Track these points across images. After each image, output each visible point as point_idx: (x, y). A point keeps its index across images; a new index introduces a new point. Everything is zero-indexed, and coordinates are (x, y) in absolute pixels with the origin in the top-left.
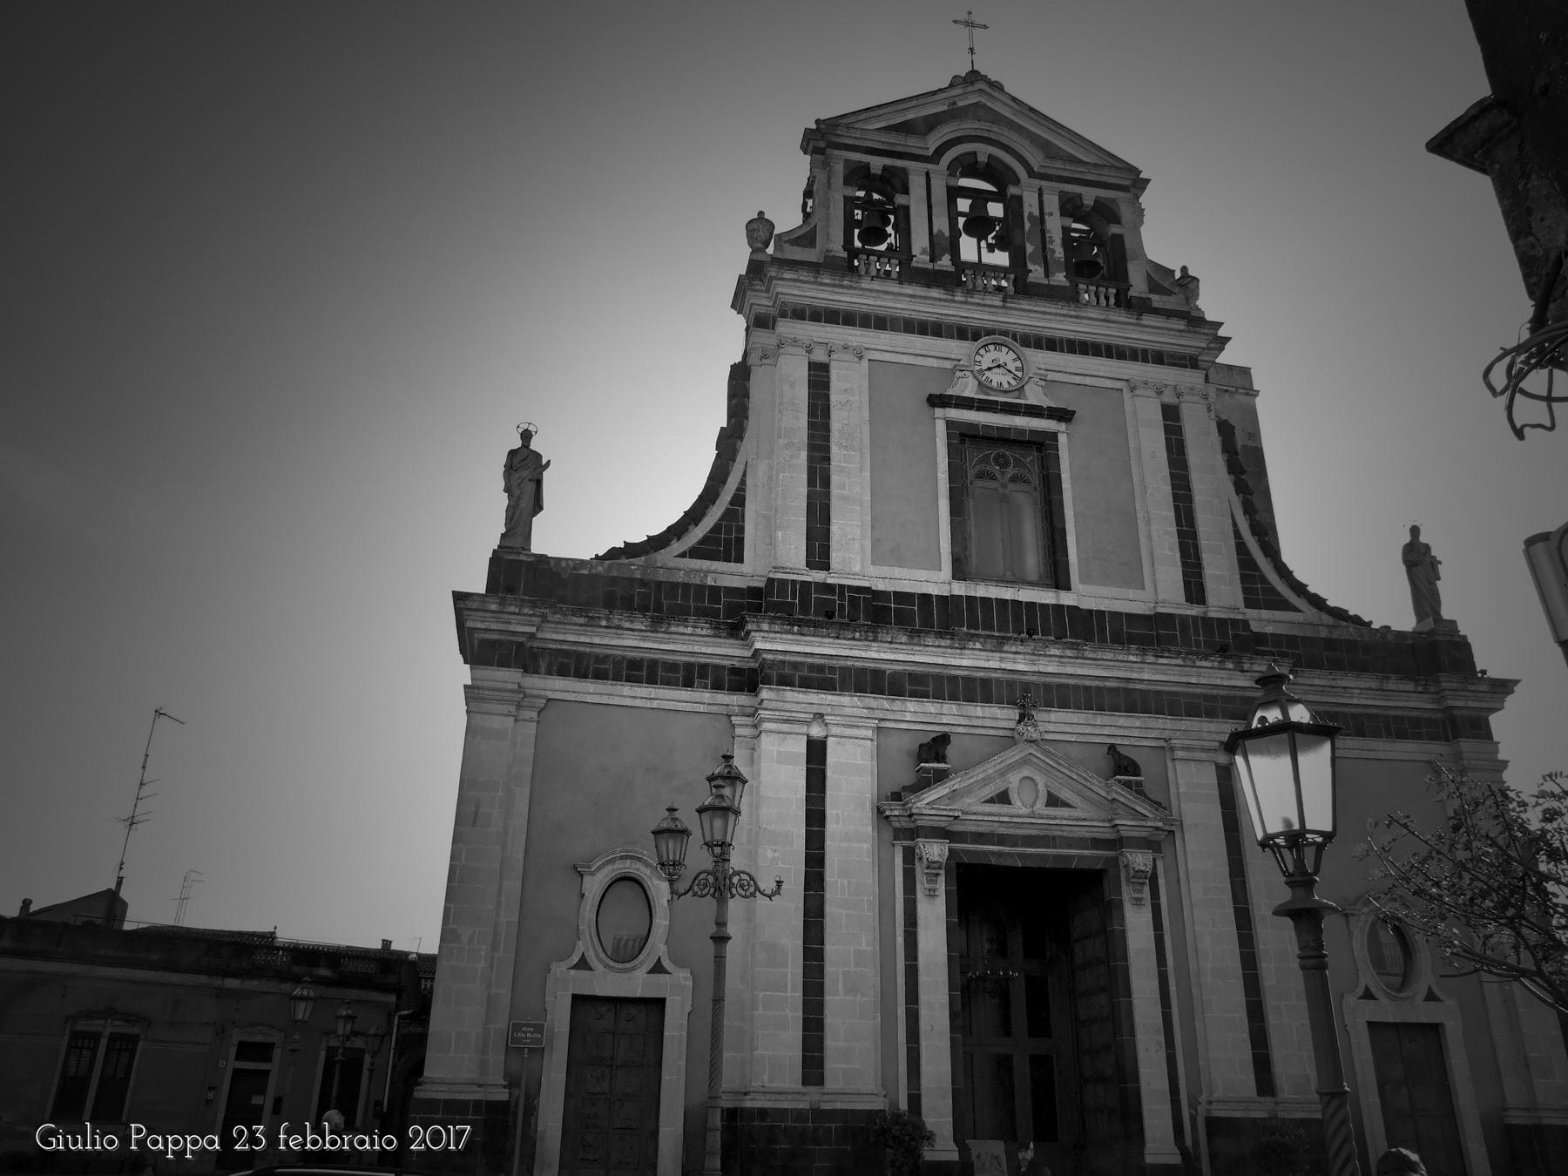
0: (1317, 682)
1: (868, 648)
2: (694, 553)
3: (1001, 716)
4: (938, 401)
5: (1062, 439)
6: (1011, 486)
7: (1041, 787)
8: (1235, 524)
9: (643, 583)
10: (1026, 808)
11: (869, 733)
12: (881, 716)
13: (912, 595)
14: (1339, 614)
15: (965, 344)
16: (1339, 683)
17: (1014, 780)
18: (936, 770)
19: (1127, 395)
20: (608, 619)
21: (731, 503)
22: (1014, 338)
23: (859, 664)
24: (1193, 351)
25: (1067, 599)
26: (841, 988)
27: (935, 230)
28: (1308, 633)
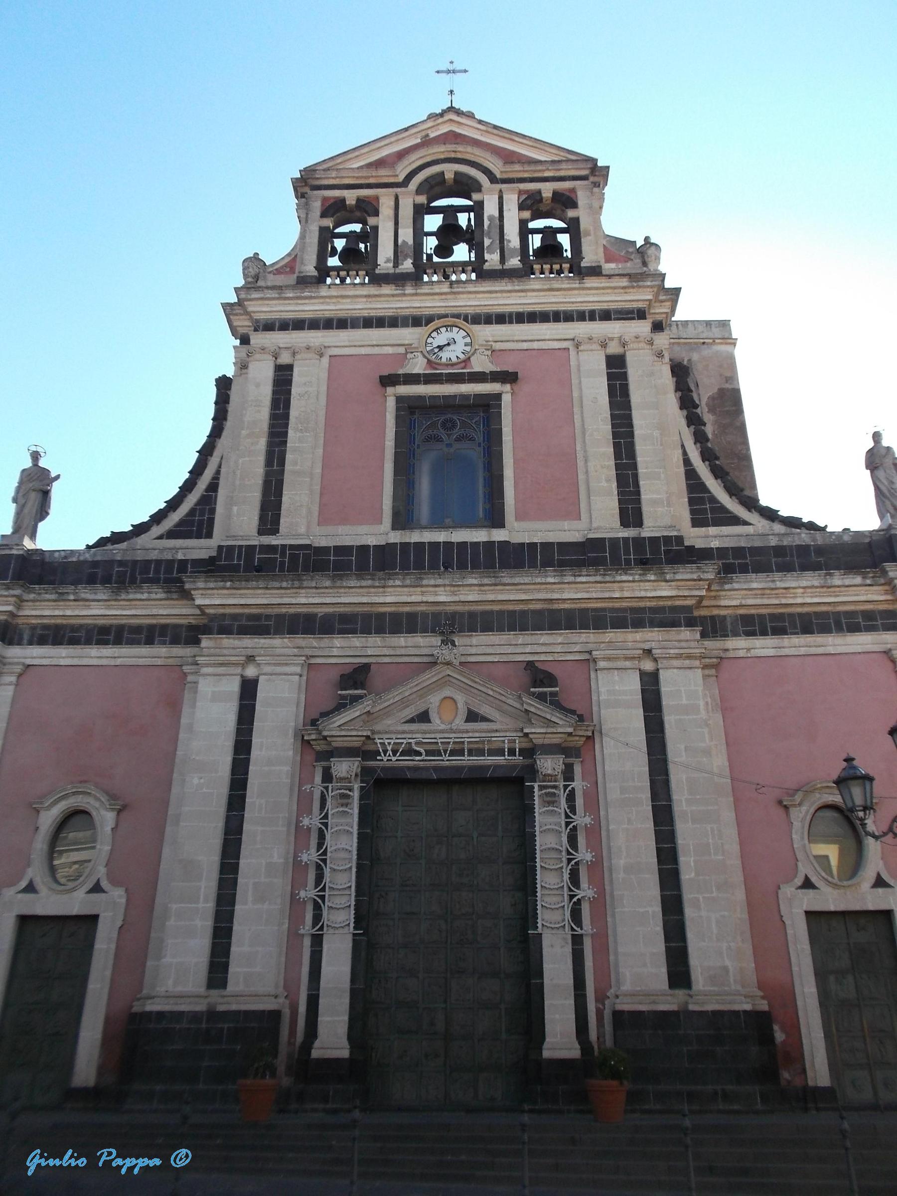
0: (755, 585)
1: (297, 594)
2: (171, 534)
3: (423, 644)
4: (388, 381)
5: (506, 399)
6: (457, 445)
7: (461, 705)
8: (685, 453)
9: (121, 563)
10: (447, 725)
11: (298, 669)
12: (310, 653)
13: (351, 548)
14: (793, 523)
15: (418, 330)
16: (779, 584)
17: (434, 700)
18: (351, 696)
19: (573, 352)
20: (75, 594)
21: (207, 490)
22: (466, 319)
23: (292, 611)
24: (640, 305)
25: (499, 535)
26: (250, 899)
27: (400, 241)
28: (758, 543)
